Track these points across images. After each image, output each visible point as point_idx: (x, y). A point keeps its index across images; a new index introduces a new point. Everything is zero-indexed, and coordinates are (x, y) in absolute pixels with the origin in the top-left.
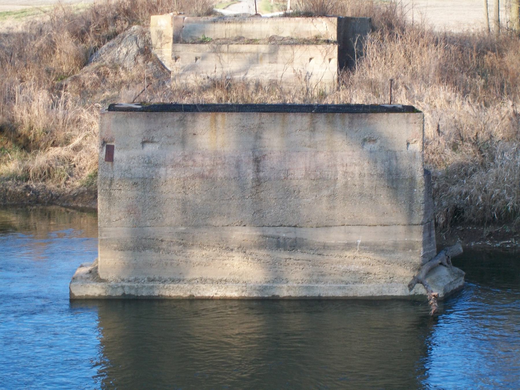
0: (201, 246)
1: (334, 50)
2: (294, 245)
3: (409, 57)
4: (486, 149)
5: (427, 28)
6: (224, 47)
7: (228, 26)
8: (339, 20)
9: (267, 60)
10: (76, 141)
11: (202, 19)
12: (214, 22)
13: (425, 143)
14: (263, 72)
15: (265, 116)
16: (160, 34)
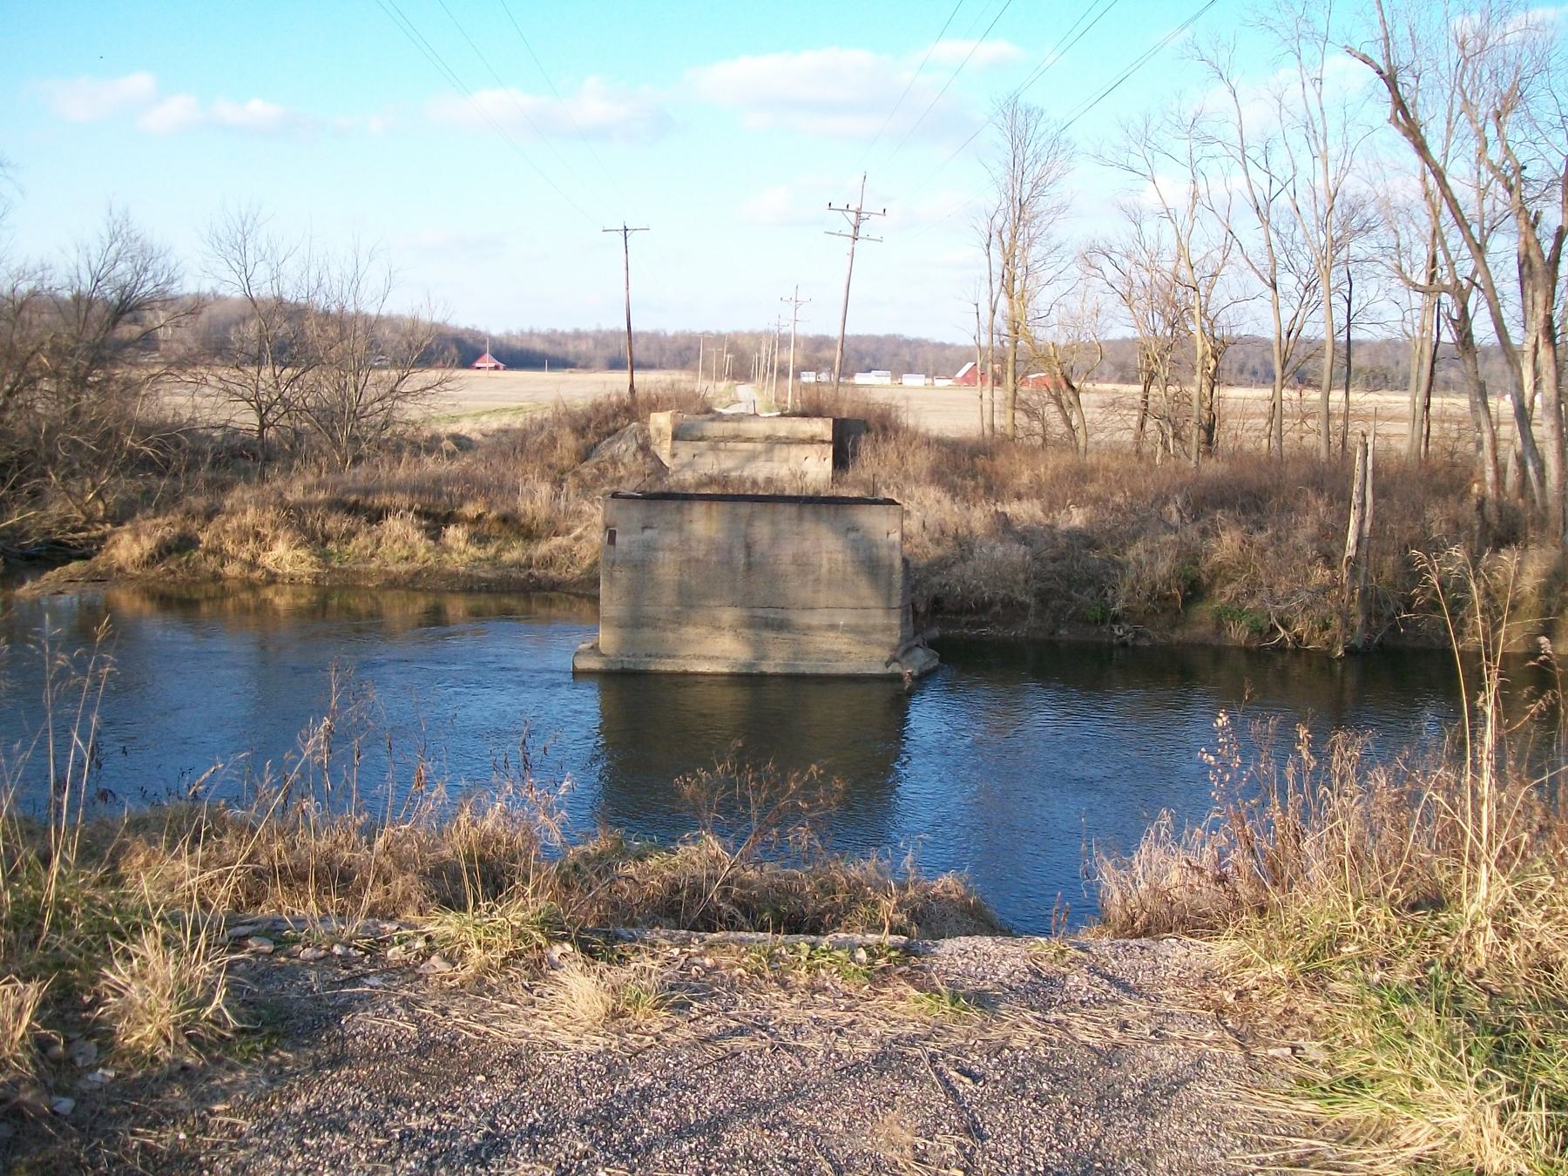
0: (695, 625)
1: (829, 450)
2: (781, 626)
3: (902, 458)
4: (964, 545)
5: (922, 430)
6: (722, 445)
7: (725, 425)
8: (835, 421)
9: (763, 457)
10: (577, 532)
11: (700, 417)
12: (712, 420)
13: (905, 537)
14: (760, 470)
15: (758, 506)
16: (659, 431)
